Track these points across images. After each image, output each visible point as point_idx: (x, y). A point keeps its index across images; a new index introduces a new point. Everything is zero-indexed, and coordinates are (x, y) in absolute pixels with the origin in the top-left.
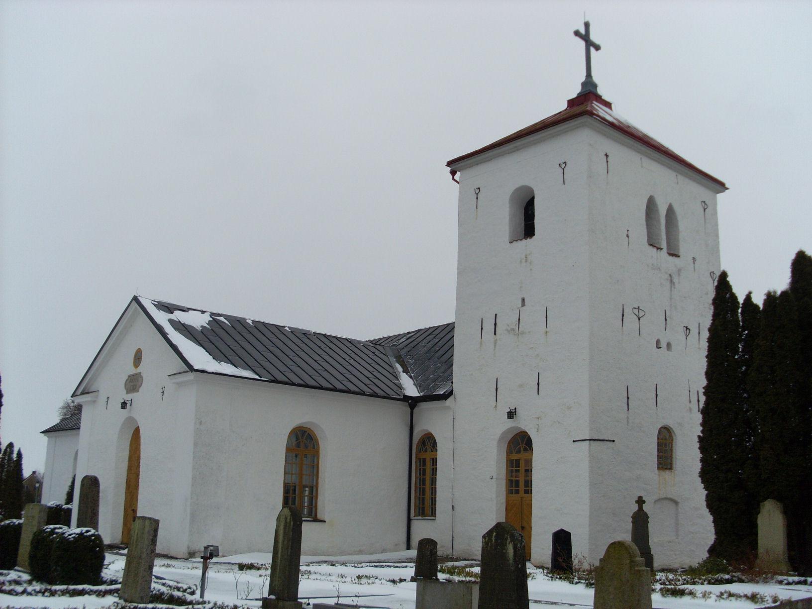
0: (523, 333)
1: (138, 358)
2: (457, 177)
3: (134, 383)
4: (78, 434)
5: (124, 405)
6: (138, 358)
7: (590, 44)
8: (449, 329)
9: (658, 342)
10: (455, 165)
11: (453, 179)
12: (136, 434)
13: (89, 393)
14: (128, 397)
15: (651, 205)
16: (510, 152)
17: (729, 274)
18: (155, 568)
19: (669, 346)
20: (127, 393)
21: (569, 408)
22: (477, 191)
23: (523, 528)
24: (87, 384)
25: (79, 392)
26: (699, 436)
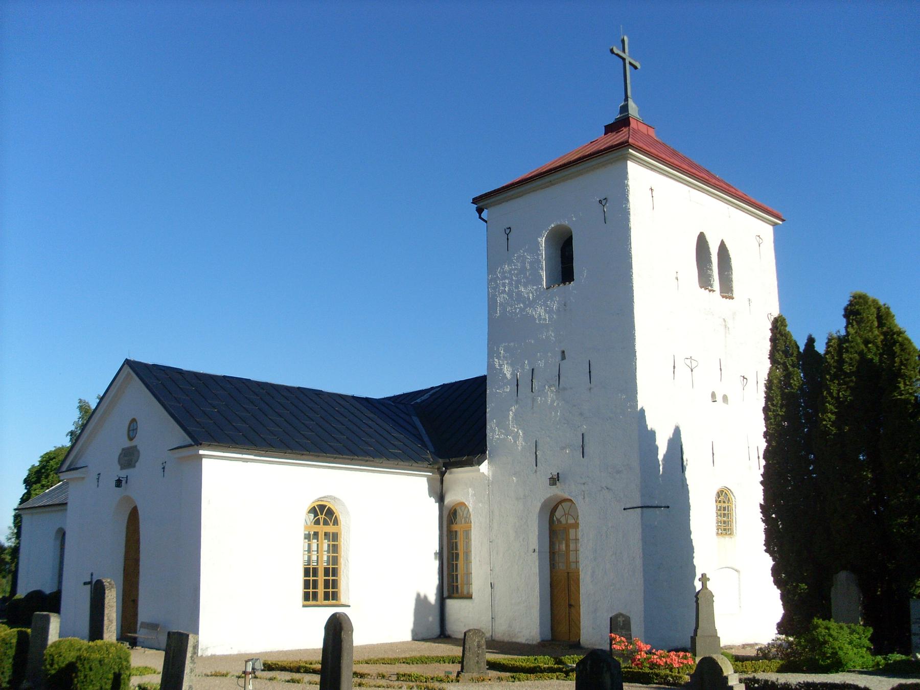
0: (565, 389)
1: (132, 430)
2: (483, 215)
3: (129, 458)
4: (66, 510)
5: (119, 483)
6: (132, 430)
7: (563, 358)
8: (484, 377)
9: (713, 395)
10: (482, 202)
11: (480, 217)
12: (133, 518)
13: (77, 469)
14: (123, 474)
15: (702, 241)
16: (542, 187)
17: (788, 322)
18: (160, 667)
19: (725, 399)
20: (122, 468)
21: (619, 472)
22: (508, 231)
23: (570, 606)
24: (76, 457)
25: (64, 468)
26: (761, 505)
